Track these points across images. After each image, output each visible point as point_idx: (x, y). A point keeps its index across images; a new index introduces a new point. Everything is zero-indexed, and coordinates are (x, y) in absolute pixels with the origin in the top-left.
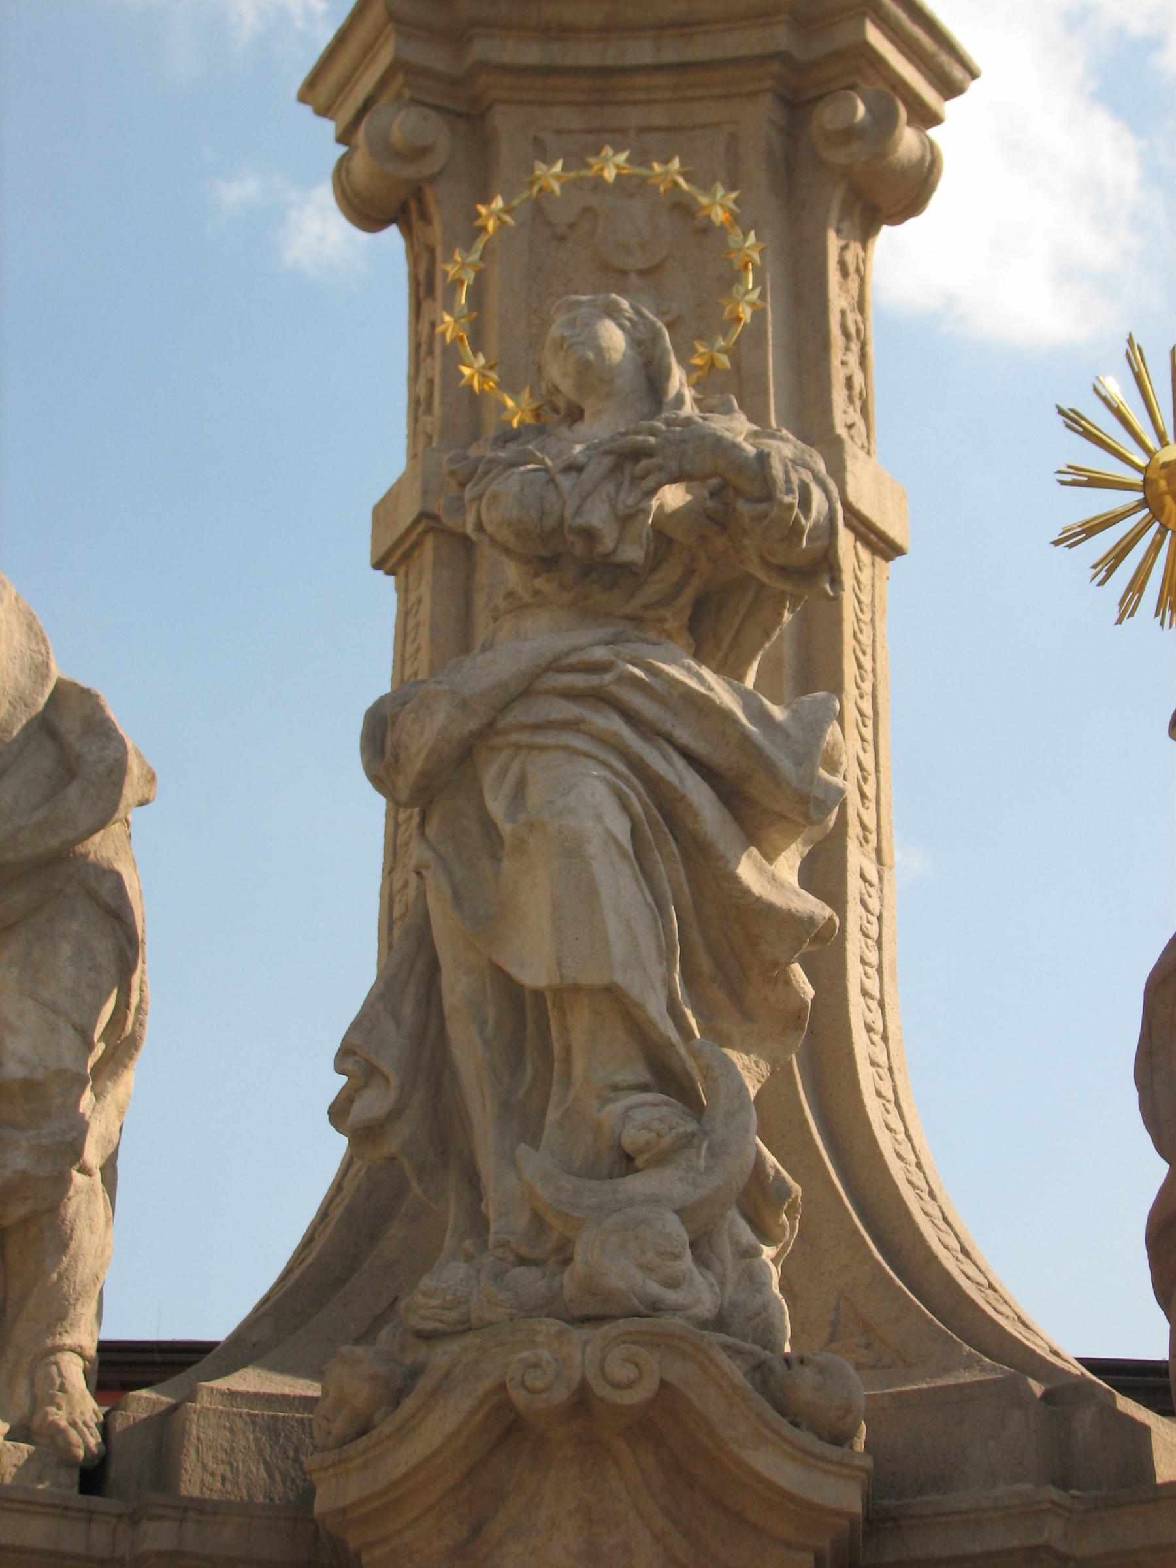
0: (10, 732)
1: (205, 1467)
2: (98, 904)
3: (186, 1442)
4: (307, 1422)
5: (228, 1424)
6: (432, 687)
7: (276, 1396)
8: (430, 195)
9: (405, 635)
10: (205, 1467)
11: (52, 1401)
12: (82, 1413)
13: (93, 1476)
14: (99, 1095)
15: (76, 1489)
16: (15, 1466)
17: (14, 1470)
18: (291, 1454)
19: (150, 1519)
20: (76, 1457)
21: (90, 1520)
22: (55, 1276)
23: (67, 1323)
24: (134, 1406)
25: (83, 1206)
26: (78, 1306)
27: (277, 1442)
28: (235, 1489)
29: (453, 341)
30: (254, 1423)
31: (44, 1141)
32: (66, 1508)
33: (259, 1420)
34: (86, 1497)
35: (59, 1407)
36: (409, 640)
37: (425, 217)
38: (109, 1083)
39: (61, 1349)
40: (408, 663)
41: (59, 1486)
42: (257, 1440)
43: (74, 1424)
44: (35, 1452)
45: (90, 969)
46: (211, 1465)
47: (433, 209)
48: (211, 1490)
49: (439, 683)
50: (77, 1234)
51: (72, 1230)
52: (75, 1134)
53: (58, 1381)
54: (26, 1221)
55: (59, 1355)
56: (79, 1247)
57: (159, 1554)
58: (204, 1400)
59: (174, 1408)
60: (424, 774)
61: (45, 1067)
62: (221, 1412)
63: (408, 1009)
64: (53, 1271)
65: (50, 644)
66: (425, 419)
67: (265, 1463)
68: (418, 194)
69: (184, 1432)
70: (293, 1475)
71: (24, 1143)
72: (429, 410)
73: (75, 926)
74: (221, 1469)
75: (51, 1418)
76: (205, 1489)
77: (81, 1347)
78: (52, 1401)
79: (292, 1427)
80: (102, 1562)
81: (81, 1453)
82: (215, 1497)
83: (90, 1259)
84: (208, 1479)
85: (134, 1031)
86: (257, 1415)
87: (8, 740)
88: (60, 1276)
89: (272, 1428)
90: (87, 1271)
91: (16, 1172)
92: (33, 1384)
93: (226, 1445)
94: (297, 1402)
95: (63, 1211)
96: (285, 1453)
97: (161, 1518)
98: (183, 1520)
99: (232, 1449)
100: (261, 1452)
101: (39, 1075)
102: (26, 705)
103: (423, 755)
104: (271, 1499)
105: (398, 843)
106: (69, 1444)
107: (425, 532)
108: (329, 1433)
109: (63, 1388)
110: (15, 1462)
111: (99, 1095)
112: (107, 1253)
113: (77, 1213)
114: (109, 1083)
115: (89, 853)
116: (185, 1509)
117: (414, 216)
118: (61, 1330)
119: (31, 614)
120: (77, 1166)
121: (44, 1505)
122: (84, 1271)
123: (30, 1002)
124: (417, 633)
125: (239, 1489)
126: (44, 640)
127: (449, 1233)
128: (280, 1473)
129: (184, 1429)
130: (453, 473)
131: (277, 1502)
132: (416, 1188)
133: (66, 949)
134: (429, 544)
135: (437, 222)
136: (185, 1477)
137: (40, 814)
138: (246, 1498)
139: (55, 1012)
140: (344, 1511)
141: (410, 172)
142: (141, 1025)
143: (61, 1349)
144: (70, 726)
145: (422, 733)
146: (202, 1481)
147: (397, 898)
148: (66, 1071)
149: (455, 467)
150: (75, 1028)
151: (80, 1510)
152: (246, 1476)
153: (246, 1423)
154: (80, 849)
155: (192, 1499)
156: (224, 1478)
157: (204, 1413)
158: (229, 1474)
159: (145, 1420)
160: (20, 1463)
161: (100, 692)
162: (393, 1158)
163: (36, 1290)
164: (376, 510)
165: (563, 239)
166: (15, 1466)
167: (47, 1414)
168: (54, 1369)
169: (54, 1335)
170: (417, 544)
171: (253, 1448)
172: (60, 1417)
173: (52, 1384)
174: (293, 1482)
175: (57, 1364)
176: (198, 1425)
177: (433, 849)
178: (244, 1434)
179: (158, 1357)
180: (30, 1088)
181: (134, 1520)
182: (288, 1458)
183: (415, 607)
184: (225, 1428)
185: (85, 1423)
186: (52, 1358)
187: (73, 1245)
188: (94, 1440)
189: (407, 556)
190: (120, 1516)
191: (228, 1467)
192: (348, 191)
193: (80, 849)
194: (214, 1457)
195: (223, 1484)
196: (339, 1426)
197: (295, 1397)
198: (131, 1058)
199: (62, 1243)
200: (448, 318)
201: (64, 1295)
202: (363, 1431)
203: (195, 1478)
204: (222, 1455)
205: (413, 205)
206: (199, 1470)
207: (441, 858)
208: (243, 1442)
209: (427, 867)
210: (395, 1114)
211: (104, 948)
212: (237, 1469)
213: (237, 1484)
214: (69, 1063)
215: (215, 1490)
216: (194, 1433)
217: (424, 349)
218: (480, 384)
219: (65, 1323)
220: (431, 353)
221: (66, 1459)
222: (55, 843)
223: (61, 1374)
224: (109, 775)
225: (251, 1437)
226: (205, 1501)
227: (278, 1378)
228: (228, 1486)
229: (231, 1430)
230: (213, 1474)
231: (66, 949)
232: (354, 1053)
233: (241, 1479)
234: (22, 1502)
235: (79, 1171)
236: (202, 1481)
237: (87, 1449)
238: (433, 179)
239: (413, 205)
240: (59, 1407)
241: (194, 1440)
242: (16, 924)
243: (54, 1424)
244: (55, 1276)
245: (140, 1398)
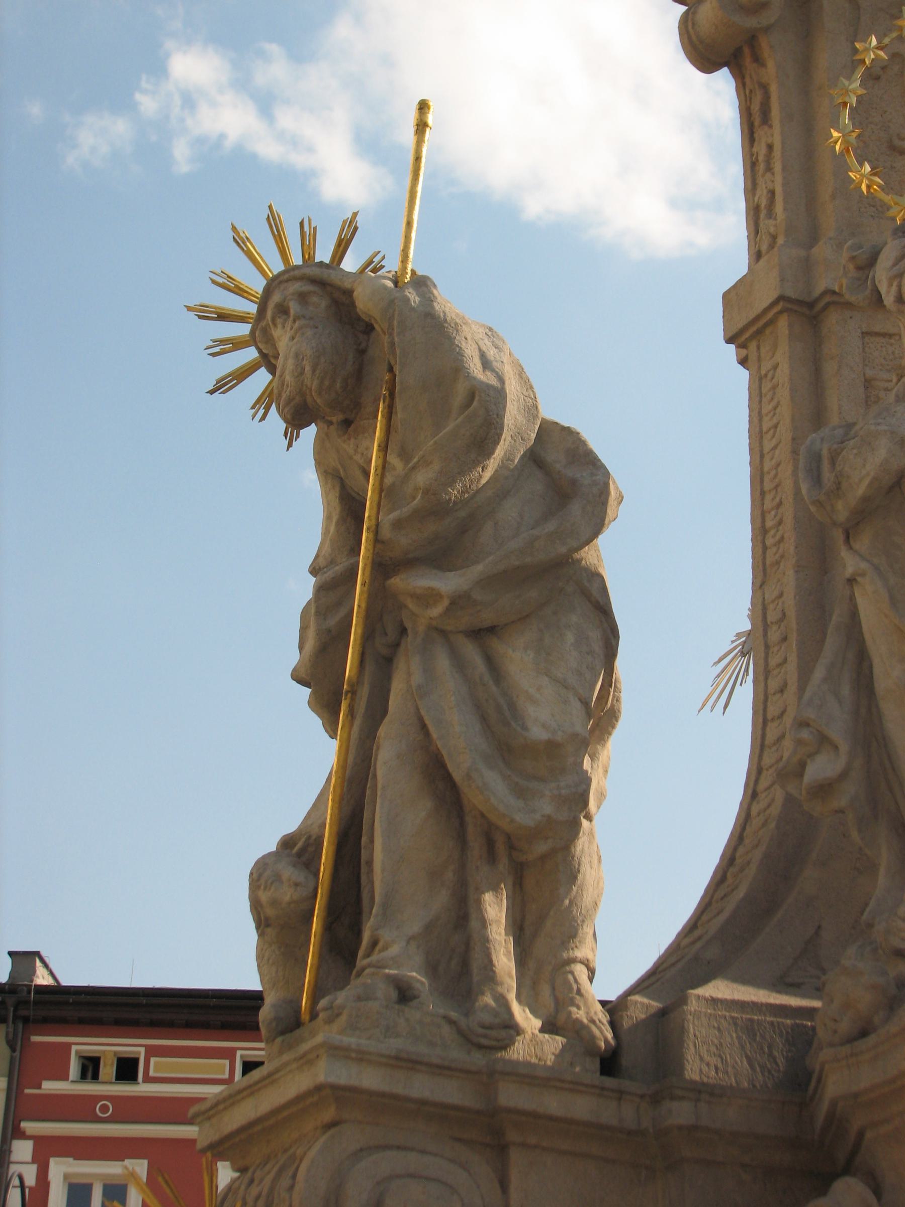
0: (513, 461)
1: (701, 1059)
2: (590, 601)
3: (686, 1038)
4: (776, 1024)
5: (716, 1025)
6: (873, 427)
7: (748, 1003)
8: (764, 42)
9: (761, 395)
10: (701, 1059)
11: (572, 1003)
12: (596, 1013)
13: (609, 1063)
14: (593, 758)
15: (598, 1073)
16: (553, 1054)
17: (553, 1057)
18: (766, 1050)
19: (673, 1098)
20: (600, 1048)
21: (620, 1099)
22: (567, 902)
23: (577, 940)
24: (632, 1008)
25: (586, 845)
26: (585, 927)
27: (755, 1040)
28: (726, 1077)
29: (841, 153)
30: (735, 1024)
31: (563, 792)
32: (603, 1089)
33: (739, 1022)
34: (604, 1078)
35: (579, 1008)
36: (764, 400)
37: (758, 60)
38: (599, 747)
39: (574, 961)
40: (766, 419)
41: (587, 1070)
42: (738, 1037)
43: (593, 1022)
44: (567, 1043)
45: (588, 653)
46: (707, 1058)
47: (766, 53)
48: (708, 1077)
49: (879, 424)
50: (582, 869)
51: (579, 865)
52: (584, 787)
53: (575, 987)
54: (543, 858)
55: (573, 965)
56: (584, 879)
57: (680, 1128)
58: (693, 1006)
59: (663, 1013)
60: (865, 499)
61: (563, 731)
62: (710, 1015)
63: (846, 690)
64: (566, 898)
65: (536, 390)
66: (764, 223)
67: (747, 1057)
68: (752, 40)
69: (683, 1030)
70: (769, 1066)
71: (547, 793)
72: (770, 214)
73: (574, 618)
74: (714, 1061)
75: (574, 1016)
76: (703, 1077)
77: (588, 960)
78: (572, 1003)
79: (765, 1028)
80: (630, 1133)
81: (603, 1045)
82: (711, 1081)
83: (591, 889)
84: (705, 1068)
85: (612, 705)
86: (737, 1018)
87: (512, 467)
88: (571, 902)
89: (750, 1029)
90: (589, 899)
91: (543, 816)
92: (554, 989)
93: (716, 1041)
94: (764, 1008)
95: (573, 850)
96: (762, 1048)
97: (682, 1098)
98: (698, 1100)
99: (721, 1044)
100: (742, 1047)
101: (559, 737)
102: (523, 439)
103: (866, 482)
104: (754, 1086)
105: (768, 562)
106: (593, 1037)
107: (781, 312)
108: (835, 1032)
109: (579, 992)
110: (553, 1050)
111: (593, 758)
112: (601, 884)
113: (582, 851)
114: (599, 747)
115: (582, 559)
116: (700, 1092)
117: (748, 61)
118: (573, 945)
119: (520, 366)
120: (583, 814)
121: (587, 1086)
122: (587, 899)
123: (546, 679)
124: (774, 394)
125: (729, 1077)
126: (531, 387)
127: (882, 871)
128: (759, 1065)
129: (683, 1027)
130: (853, 258)
131: (758, 1087)
132: (855, 835)
133: (570, 637)
134: (783, 323)
135: (771, 64)
136: (688, 1067)
137: (551, 526)
138: (734, 1084)
139: (566, 688)
140: (856, 1095)
141: (751, 22)
142: (617, 700)
143: (574, 961)
144: (555, 457)
145: (864, 465)
146: (701, 1070)
147: (771, 607)
148: (578, 735)
149: (855, 254)
150: (580, 700)
151: (613, 1091)
152: (733, 1067)
153: (729, 1024)
154: (576, 556)
155: (693, 1082)
156: (717, 1068)
157: (697, 1015)
158: (720, 1065)
159: (644, 1020)
160: (557, 1052)
161: (579, 429)
162: (842, 811)
163: (552, 913)
164: (726, 296)
165: (877, 78)
166: (553, 1054)
167: (570, 1013)
168: (570, 977)
169: (568, 950)
170: (771, 322)
171: (737, 1044)
172: (580, 1014)
173: (571, 989)
174: (769, 1072)
175: (572, 973)
176: (693, 1024)
177: (868, 561)
178: (729, 1033)
179: (144, 1000)
180: (552, 748)
181: (656, 1099)
182: (764, 1052)
183: (771, 372)
184: (714, 1027)
185: (600, 1021)
186: (568, 968)
187: (580, 876)
188: (609, 1035)
189: (759, 332)
190: (642, 1097)
191: (719, 1060)
192: (694, 38)
193: (576, 556)
194: (707, 1053)
195: (717, 1073)
196: (845, 1026)
197: (762, 1004)
198: (613, 727)
199: (573, 875)
200: (835, 134)
201: (573, 917)
202: (864, 1033)
203: (697, 1065)
204: (713, 1049)
205: (746, 51)
206: (698, 1061)
207: (876, 568)
208: (728, 1039)
209: (863, 575)
210: (843, 776)
211: (595, 635)
212: (726, 1061)
213: (727, 1072)
214: (578, 728)
215: (711, 1076)
216: (692, 1030)
217: (761, 167)
218: (868, 187)
219: (575, 940)
220: (769, 169)
221: (590, 1049)
222: (563, 550)
223: (576, 981)
224: (600, 496)
225: (734, 1035)
226: (703, 1084)
227: (743, 988)
228: (721, 1075)
229: (719, 1029)
230: (708, 1065)
231: (570, 637)
232: (808, 725)
233: (730, 1069)
234: (571, 1082)
235: (584, 817)
236: (701, 1070)
237: (606, 1041)
238: (767, 29)
239: (746, 51)
240: (579, 1008)
241: (691, 1036)
242: (527, 616)
243: (578, 1021)
244: (567, 902)
245: (636, 1002)
